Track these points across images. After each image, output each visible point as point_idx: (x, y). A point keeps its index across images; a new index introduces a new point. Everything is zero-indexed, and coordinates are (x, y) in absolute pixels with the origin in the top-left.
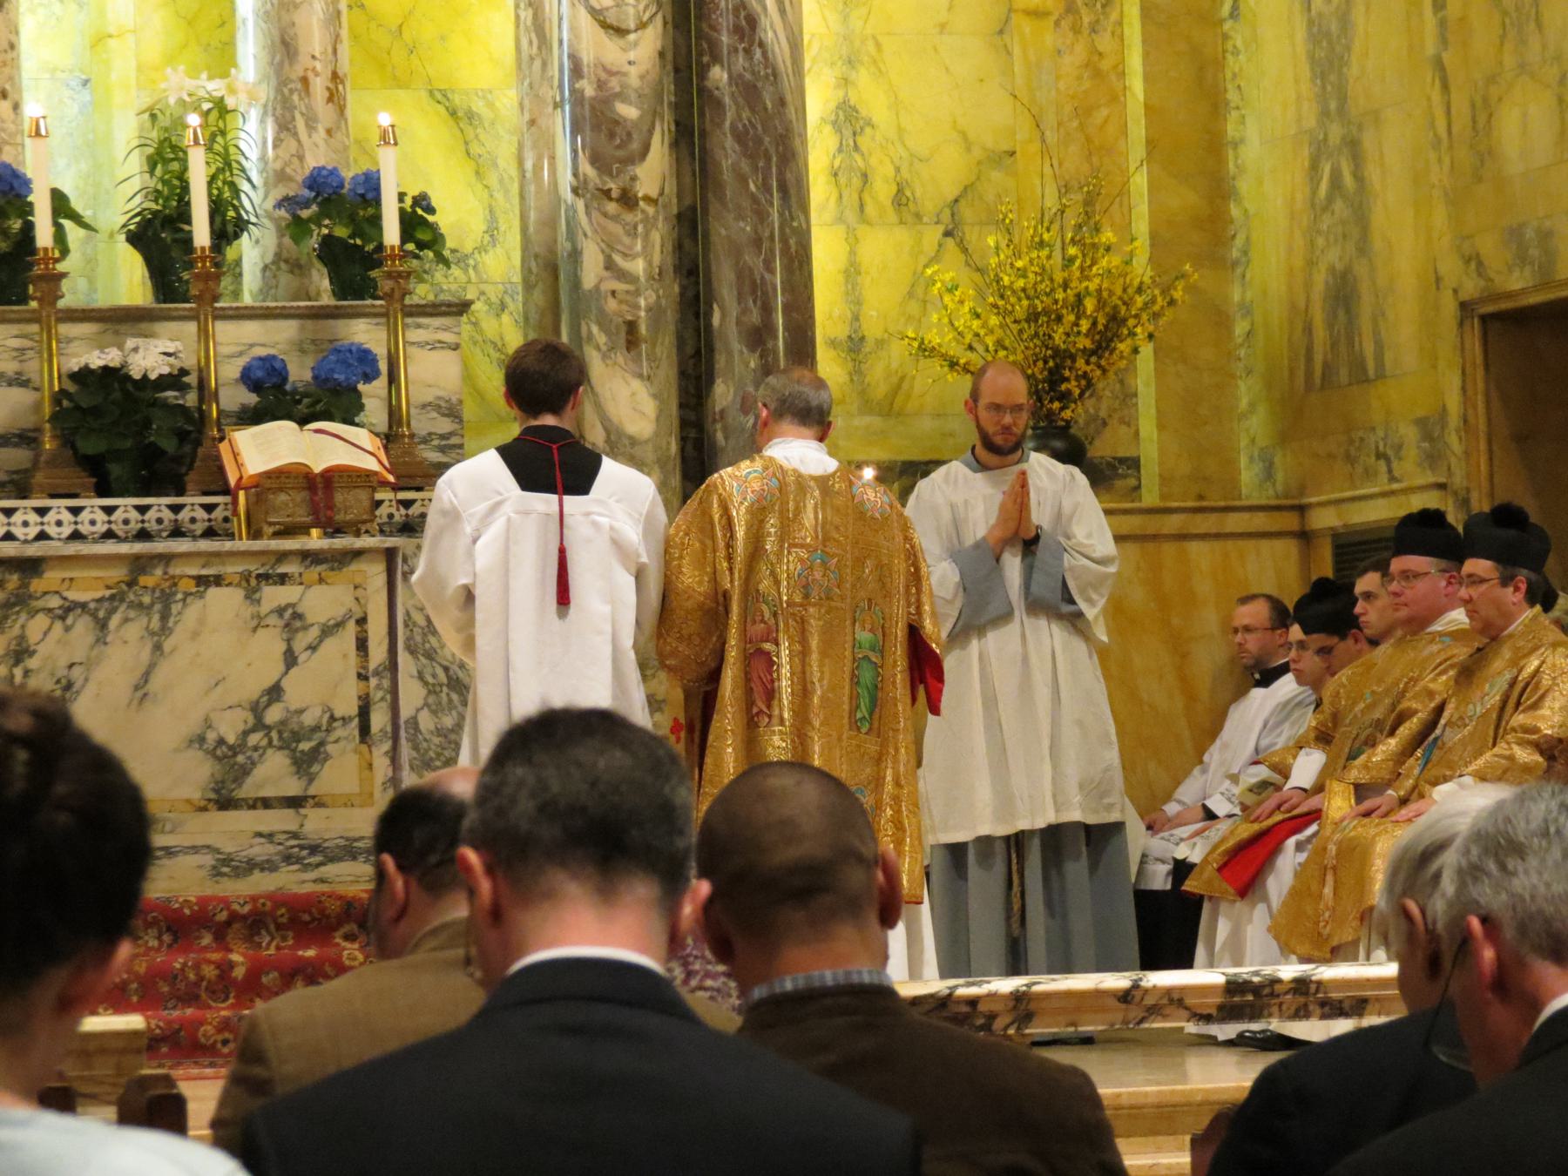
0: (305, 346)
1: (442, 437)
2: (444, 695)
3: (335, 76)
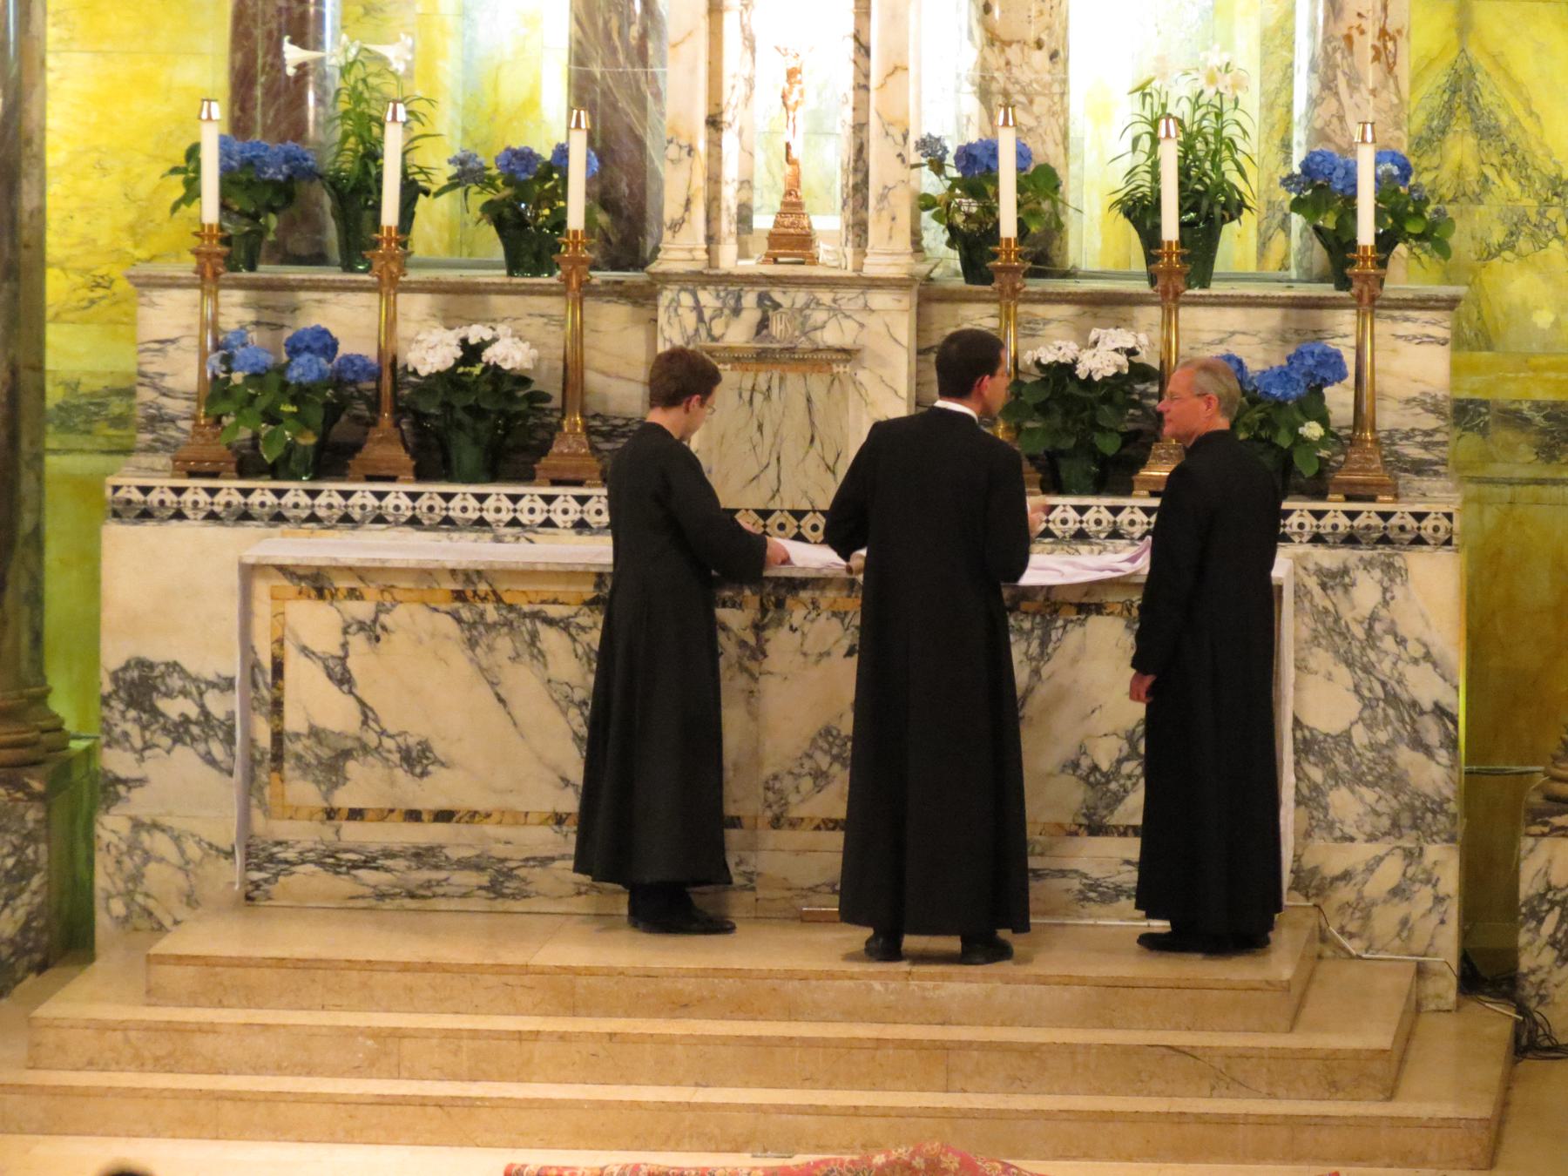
0: (1288, 336)
1: (1426, 433)
2: (1380, 711)
3: (1383, 33)
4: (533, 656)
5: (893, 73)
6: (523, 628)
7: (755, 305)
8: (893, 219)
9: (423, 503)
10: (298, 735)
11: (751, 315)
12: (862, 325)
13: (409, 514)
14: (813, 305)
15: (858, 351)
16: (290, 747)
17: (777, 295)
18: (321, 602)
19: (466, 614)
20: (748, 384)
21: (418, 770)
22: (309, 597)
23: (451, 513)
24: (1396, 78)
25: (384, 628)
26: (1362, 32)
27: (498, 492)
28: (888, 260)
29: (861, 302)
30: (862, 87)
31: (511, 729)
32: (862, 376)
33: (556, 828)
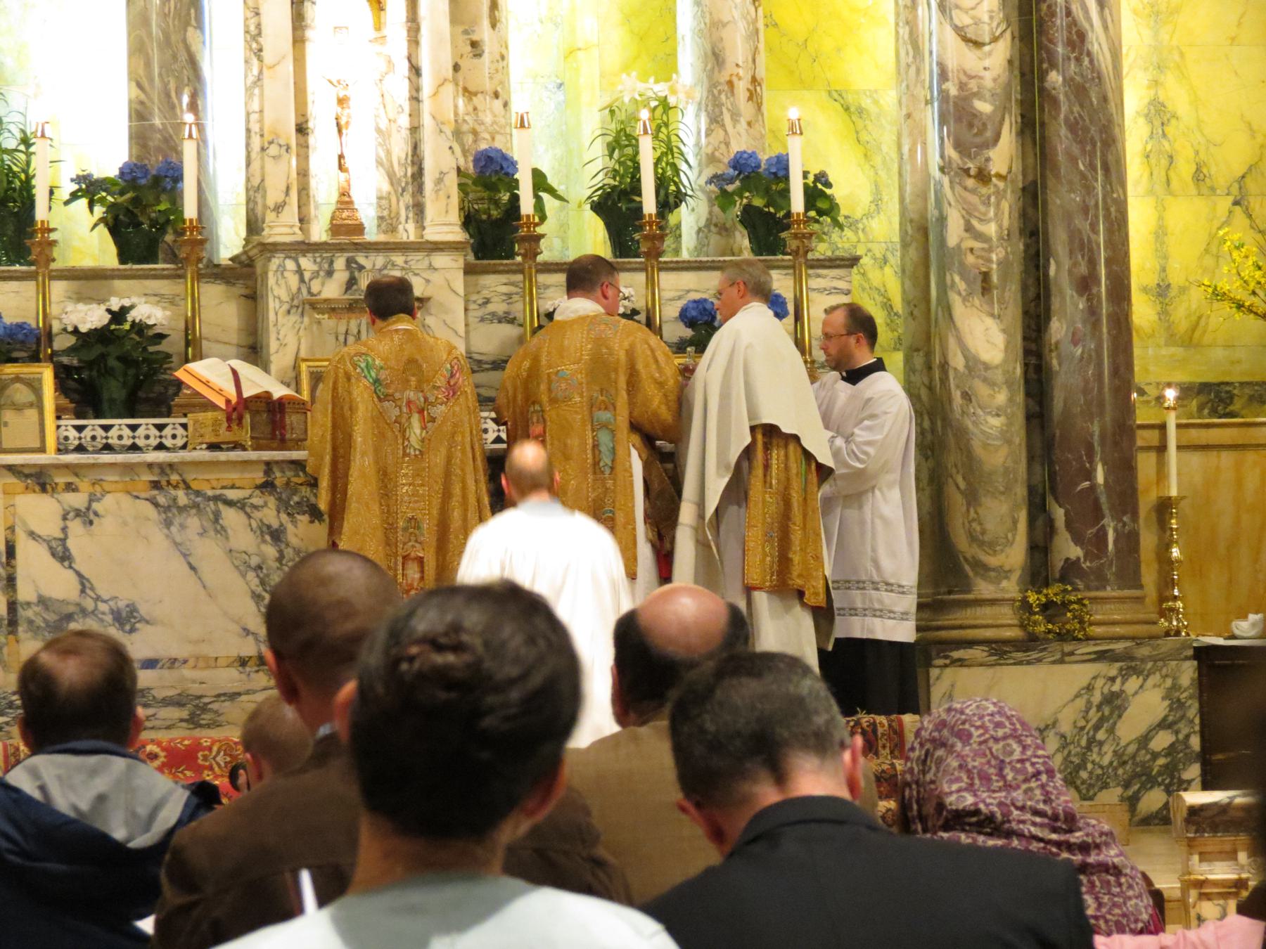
3: (754, 80)
4: (217, 532)
5: (443, 84)
6: (208, 509)
7: (344, 268)
8: (449, 197)
9: (87, 433)
10: (28, 604)
11: (341, 276)
12: (428, 281)
13: (77, 442)
14: (389, 267)
15: (428, 299)
16: (23, 614)
17: (361, 259)
18: (44, 495)
19: (161, 500)
20: (342, 329)
21: (128, 627)
22: (34, 491)
23: (110, 441)
24: (762, 115)
25: (96, 514)
26: (740, 79)
27: (146, 425)
28: (446, 229)
29: (426, 263)
30: (415, 99)
31: (202, 591)
32: (430, 321)
33: (240, 669)
